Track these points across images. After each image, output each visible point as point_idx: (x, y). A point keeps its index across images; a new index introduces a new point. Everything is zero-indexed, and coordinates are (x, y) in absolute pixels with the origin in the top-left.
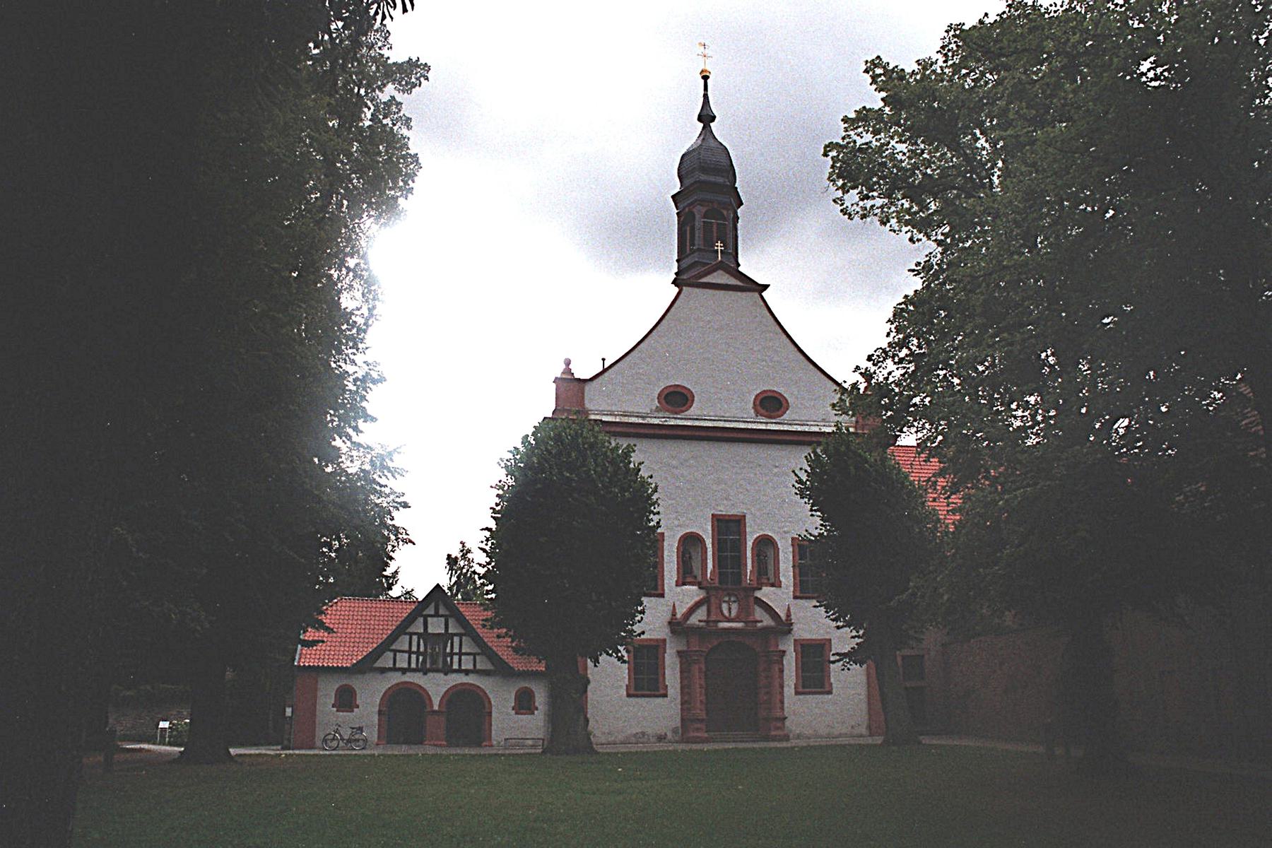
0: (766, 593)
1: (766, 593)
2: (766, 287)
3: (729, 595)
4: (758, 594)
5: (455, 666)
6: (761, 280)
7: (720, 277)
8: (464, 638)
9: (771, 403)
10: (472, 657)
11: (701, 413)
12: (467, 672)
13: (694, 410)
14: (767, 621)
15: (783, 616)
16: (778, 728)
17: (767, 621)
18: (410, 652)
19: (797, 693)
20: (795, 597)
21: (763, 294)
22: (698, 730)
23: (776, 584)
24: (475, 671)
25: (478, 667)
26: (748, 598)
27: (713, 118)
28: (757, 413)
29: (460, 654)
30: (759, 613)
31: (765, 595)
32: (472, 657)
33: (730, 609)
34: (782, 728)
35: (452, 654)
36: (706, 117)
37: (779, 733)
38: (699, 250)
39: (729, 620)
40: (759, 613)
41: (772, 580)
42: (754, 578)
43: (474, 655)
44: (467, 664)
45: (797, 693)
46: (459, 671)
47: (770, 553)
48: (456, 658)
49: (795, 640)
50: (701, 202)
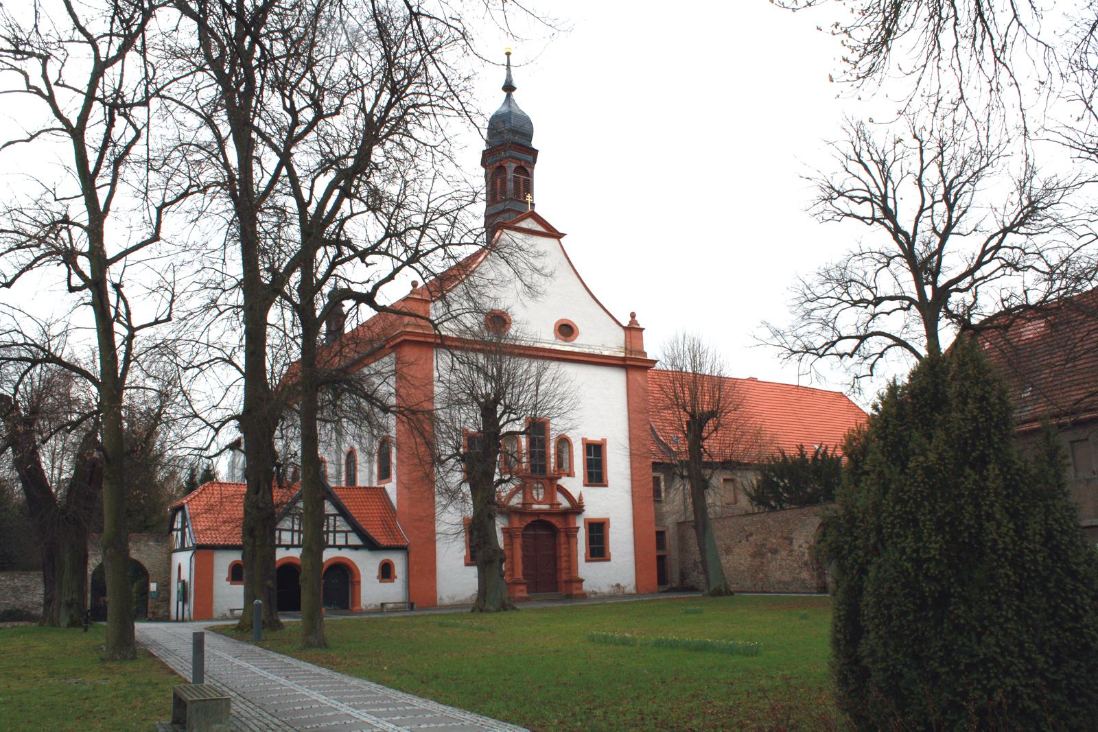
0: (564, 482)
1: (564, 482)
2: (563, 235)
3: (538, 483)
4: (560, 482)
5: (331, 542)
6: (561, 231)
7: (529, 224)
8: (338, 518)
9: (566, 330)
10: (344, 534)
11: (583, 343)
12: (340, 547)
13: (578, 341)
14: (565, 504)
15: (576, 497)
16: (577, 588)
17: (565, 504)
18: (293, 531)
19: (587, 561)
20: (585, 485)
21: (561, 240)
22: (522, 591)
23: (570, 474)
24: (347, 546)
25: (350, 543)
26: (551, 484)
27: (513, 89)
28: (557, 337)
29: (335, 532)
30: (560, 498)
31: (564, 483)
32: (344, 534)
33: (538, 494)
34: (581, 588)
35: (328, 532)
36: (509, 88)
37: (578, 592)
38: (511, 199)
39: (539, 503)
40: (560, 498)
41: (567, 471)
42: (556, 469)
43: (346, 532)
44: (340, 540)
45: (587, 561)
46: (334, 546)
47: (566, 449)
48: (331, 535)
49: (585, 519)
50: (514, 158)
